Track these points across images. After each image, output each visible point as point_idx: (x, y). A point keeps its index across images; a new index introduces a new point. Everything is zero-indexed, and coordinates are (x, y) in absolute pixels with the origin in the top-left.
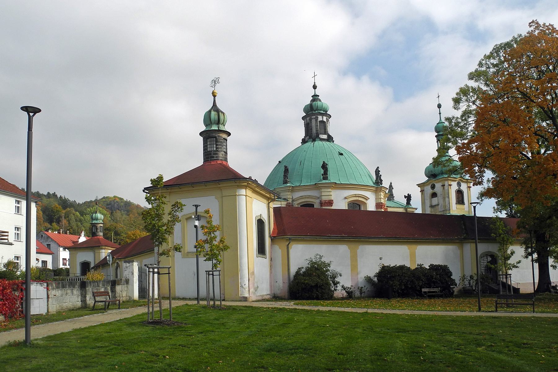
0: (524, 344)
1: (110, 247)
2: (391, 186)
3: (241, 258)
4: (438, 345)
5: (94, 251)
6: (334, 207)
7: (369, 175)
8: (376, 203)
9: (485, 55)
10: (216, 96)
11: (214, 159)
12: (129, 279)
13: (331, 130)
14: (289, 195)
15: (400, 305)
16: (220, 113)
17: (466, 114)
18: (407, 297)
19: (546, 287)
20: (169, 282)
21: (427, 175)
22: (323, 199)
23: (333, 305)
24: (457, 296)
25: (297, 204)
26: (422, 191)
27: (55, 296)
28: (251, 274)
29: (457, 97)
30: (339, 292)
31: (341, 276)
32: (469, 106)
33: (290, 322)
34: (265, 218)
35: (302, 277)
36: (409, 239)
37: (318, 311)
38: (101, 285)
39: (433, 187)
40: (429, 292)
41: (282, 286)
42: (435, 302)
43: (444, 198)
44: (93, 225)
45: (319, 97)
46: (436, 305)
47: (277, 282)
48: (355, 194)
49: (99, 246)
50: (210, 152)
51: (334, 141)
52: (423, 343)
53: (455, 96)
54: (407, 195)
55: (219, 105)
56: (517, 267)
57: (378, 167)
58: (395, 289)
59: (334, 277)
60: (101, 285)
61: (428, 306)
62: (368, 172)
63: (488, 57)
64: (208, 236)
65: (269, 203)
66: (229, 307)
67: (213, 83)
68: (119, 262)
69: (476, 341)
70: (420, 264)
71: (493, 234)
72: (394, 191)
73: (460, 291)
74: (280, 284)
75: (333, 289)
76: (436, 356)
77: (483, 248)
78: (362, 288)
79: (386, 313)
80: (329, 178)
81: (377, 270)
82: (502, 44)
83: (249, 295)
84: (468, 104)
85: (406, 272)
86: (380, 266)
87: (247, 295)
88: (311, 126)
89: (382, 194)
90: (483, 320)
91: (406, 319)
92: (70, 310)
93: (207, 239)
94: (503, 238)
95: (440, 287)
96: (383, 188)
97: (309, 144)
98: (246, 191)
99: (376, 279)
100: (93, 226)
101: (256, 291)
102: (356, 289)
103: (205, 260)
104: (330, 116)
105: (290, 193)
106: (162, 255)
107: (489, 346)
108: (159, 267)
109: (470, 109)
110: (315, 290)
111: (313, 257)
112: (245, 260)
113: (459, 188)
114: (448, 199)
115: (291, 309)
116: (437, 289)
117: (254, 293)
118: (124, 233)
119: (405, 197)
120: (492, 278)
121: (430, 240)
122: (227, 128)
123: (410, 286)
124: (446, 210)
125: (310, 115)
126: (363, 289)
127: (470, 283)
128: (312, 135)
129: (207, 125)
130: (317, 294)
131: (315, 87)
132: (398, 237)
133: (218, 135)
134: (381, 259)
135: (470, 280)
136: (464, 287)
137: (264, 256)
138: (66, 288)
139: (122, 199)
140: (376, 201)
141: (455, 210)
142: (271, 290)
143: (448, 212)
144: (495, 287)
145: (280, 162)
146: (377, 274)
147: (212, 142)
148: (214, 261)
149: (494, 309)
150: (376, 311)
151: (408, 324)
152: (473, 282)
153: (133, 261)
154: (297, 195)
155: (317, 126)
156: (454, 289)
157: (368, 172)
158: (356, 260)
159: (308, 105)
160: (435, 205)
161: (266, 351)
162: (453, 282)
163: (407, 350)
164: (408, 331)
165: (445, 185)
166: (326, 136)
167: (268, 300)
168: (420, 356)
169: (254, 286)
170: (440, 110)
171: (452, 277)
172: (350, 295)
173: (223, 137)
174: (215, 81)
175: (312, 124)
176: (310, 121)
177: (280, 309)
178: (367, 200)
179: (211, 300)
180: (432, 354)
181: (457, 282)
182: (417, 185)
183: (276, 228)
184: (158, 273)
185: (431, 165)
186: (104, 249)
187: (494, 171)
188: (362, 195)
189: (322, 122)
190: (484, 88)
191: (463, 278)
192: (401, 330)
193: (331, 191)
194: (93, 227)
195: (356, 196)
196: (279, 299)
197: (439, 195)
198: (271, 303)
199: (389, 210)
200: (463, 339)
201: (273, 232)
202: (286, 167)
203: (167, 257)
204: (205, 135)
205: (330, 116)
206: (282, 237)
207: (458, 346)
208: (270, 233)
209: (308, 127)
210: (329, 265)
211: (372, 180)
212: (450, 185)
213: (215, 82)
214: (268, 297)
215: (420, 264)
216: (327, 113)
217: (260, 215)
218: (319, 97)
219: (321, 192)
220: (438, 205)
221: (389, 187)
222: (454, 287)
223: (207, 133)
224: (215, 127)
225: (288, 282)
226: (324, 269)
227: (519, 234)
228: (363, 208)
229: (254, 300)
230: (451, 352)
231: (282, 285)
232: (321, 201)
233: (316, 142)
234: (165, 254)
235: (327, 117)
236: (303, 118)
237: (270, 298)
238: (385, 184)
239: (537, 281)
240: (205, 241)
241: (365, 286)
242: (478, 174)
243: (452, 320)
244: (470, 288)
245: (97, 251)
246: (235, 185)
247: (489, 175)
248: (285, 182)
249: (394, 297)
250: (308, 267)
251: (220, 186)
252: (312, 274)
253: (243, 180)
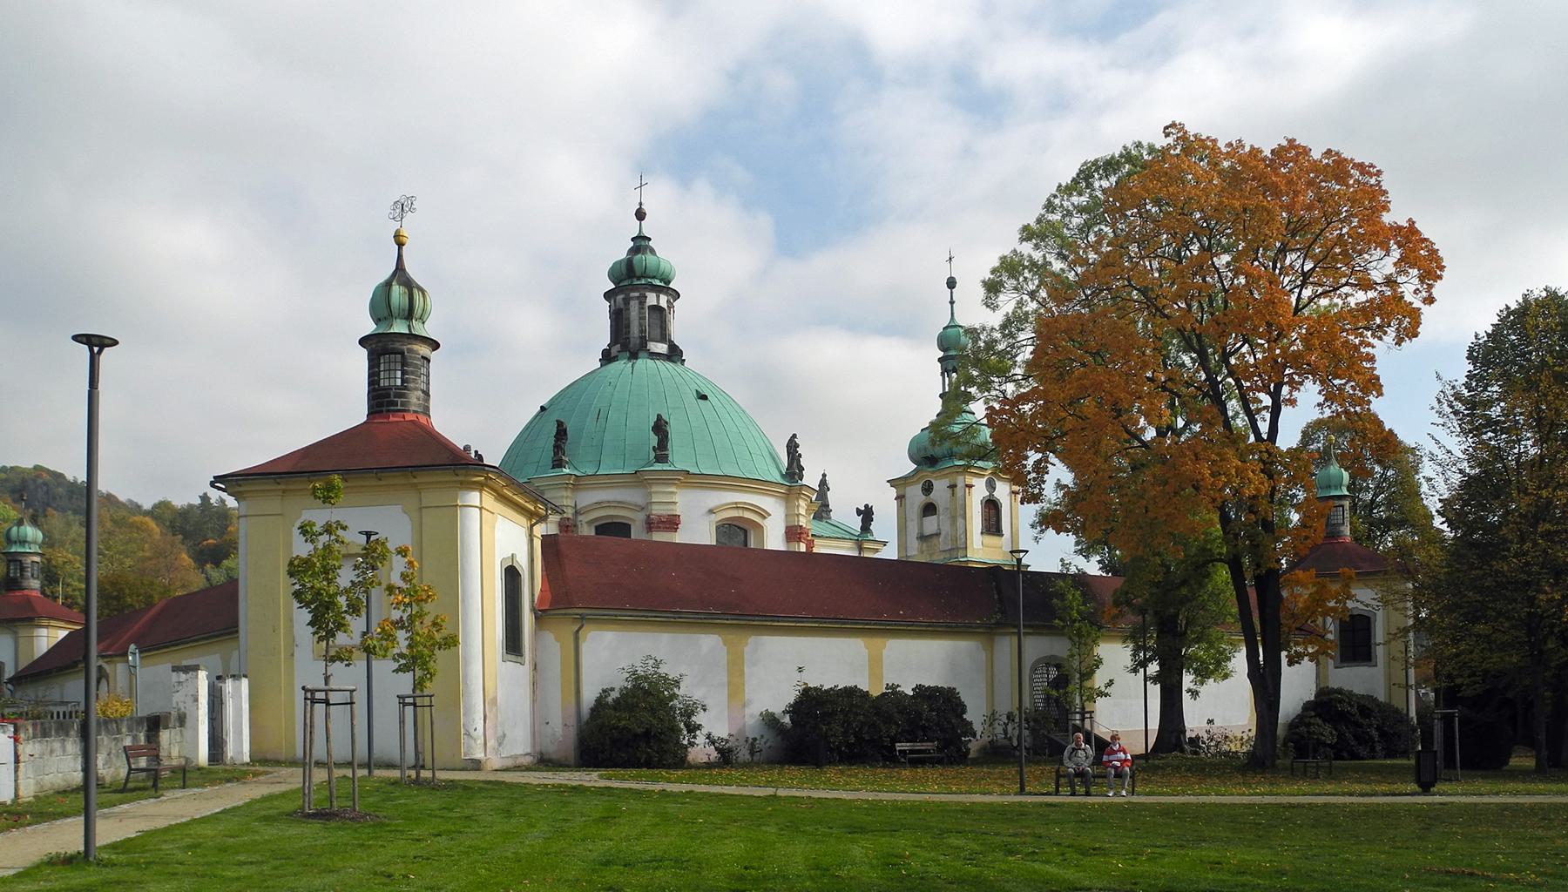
0: (1094, 849)
1: (62, 621)
2: (823, 483)
3: (466, 664)
4: (933, 854)
5: (16, 633)
6: (680, 537)
7: (770, 453)
8: (787, 528)
9: (1060, 186)
10: (403, 245)
11: (396, 408)
12: (185, 714)
13: (677, 333)
14: (567, 497)
15: (848, 779)
16: (415, 291)
17: (1010, 325)
18: (862, 763)
19: (1174, 741)
20: (352, 724)
21: (915, 457)
22: (654, 512)
23: (691, 780)
24: (976, 762)
25: (587, 523)
26: (900, 498)
27: (32, 758)
28: (490, 702)
29: (993, 279)
30: (701, 752)
31: (705, 710)
32: (1020, 304)
33: (616, 815)
34: (522, 563)
35: (612, 712)
36: (867, 624)
37: (663, 793)
38: (124, 730)
39: (928, 488)
40: (912, 752)
41: (560, 732)
42: (925, 774)
43: (954, 519)
44: (10, 558)
45: (651, 243)
46: (927, 781)
47: (547, 723)
48: (736, 503)
49: (32, 619)
50: (386, 389)
51: (684, 360)
52: (905, 850)
53: (988, 276)
54: (863, 509)
55: (411, 269)
56: (1106, 695)
57: (794, 436)
58: (834, 743)
59: (688, 713)
60: (124, 730)
61: (911, 782)
62: (768, 444)
63: (1067, 190)
64: (404, 611)
65: (532, 526)
66: (452, 785)
67: (397, 211)
68: (106, 666)
69: (1006, 846)
70: (893, 684)
71: (1057, 621)
72: (831, 497)
73: (983, 749)
74: (556, 730)
75: (685, 742)
76: (930, 869)
77: (1037, 647)
78: (755, 739)
79: (819, 798)
80: (670, 458)
81: (791, 696)
82: (1096, 161)
83: (486, 756)
84: (1018, 299)
85: (859, 704)
86: (799, 688)
87: (479, 755)
88: (628, 319)
89: (802, 503)
90: (1026, 809)
91: (865, 808)
92: (59, 793)
93: (401, 617)
94: (1079, 629)
95: (938, 739)
96: (804, 488)
97: (621, 366)
98: (481, 495)
99: (787, 720)
100: (10, 561)
101: (500, 744)
102: (742, 741)
103: (396, 671)
104: (677, 295)
105: (569, 493)
106: (334, 661)
107: (1028, 854)
108: (327, 688)
109: (1025, 309)
110: (643, 745)
111: (638, 664)
112: (476, 669)
113: (991, 495)
114: (963, 521)
115: (600, 788)
116: (931, 744)
117: (497, 751)
118: (75, 578)
119: (859, 512)
120: (1057, 720)
121: (917, 626)
122: (428, 329)
123: (1104, 760)
124: (958, 548)
125: (625, 288)
126: (758, 742)
127: (1005, 732)
128: (629, 342)
129: (379, 320)
130: (648, 753)
131: (640, 215)
132: (842, 617)
133: (409, 346)
134: (800, 670)
135: (1006, 725)
136: (992, 740)
137: (519, 659)
138: (50, 736)
139: (61, 476)
140: (787, 521)
141: (981, 550)
142: (534, 745)
143: (961, 553)
144: (1063, 740)
145: (543, 408)
146: (791, 706)
147: (392, 365)
148: (419, 673)
149: (1052, 788)
150: (794, 792)
151: (870, 818)
152: (1014, 728)
153: (196, 668)
154: (587, 498)
155: (642, 318)
156: (969, 746)
157: (768, 444)
158: (742, 674)
159: (621, 261)
160: (931, 536)
161: (602, 865)
162: (968, 729)
163: (874, 862)
164: (872, 831)
165: (956, 486)
166: (666, 346)
167: (528, 769)
168: (899, 869)
169: (496, 732)
170: (952, 293)
171: (965, 716)
172: (726, 757)
173: (421, 353)
174: (403, 205)
175: (629, 314)
176: (625, 304)
177: (574, 788)
178: (765, 518)
179: (361, 766)
180: (923, 866)
181: (978, 727)
182: (888, 481)
183: (548, 589)
184: (414, 705)
185: (927, 432)
186: (47, 627)
187: (1072, 467)
188: (752, 505)
189: (657, 309)
190: (1057, 266)
191: (992, 719)
192: (857, 829)
193: (675, 490)
194: (12, 564)
195: (737, 506)
196: (553, 767)
197: (940, 509)
198: (537, 774)
199: (821, 548)
200: (981, 844)
201: (541, 598)
202: (560, 424)
203: (346, 665)
204: (374, 346)
205: (677, 295)
206: (563, 612)
207: (970, 854)
208: (533, 601)
209: (618, 319)
210: (677, 683)
211: (778, 468)
212: (970, 486)
213: (403, 208)
214: (527, 760)
215: (893, 684)
216: (670, 286)
217: (510, 555)
218: (651, 243)
219: (650, 493)
220: (938, 535)
221: (819, 486)
222: (970, 740)
223: (380, 341)
224: (399, 327)
225: (575, 725)
226: (666, 693)
227: (1118, 618)
228: (754, 543)
229: (496, 767)
230: (959, 864)
231: (561, 730)
232: (648, 516)
233: (640, 361)
234: (342, 660)
235: (670, 297)
236: (608, 295)
237: (532, 762)
238: (811, 479)
239: (1154, 725)
240: (397, 623)
241: (762, 736)
242: (1034, 475)
243: (962, 811)
244: (1006, 742)
245: (23, 632)
246: (455, 482)
247: (1059, 474)
248: (558, 464)
249: (830, 763)
250: (626, 688)
251: (415, 481)
252: (638, 706)
253: (475, 469)
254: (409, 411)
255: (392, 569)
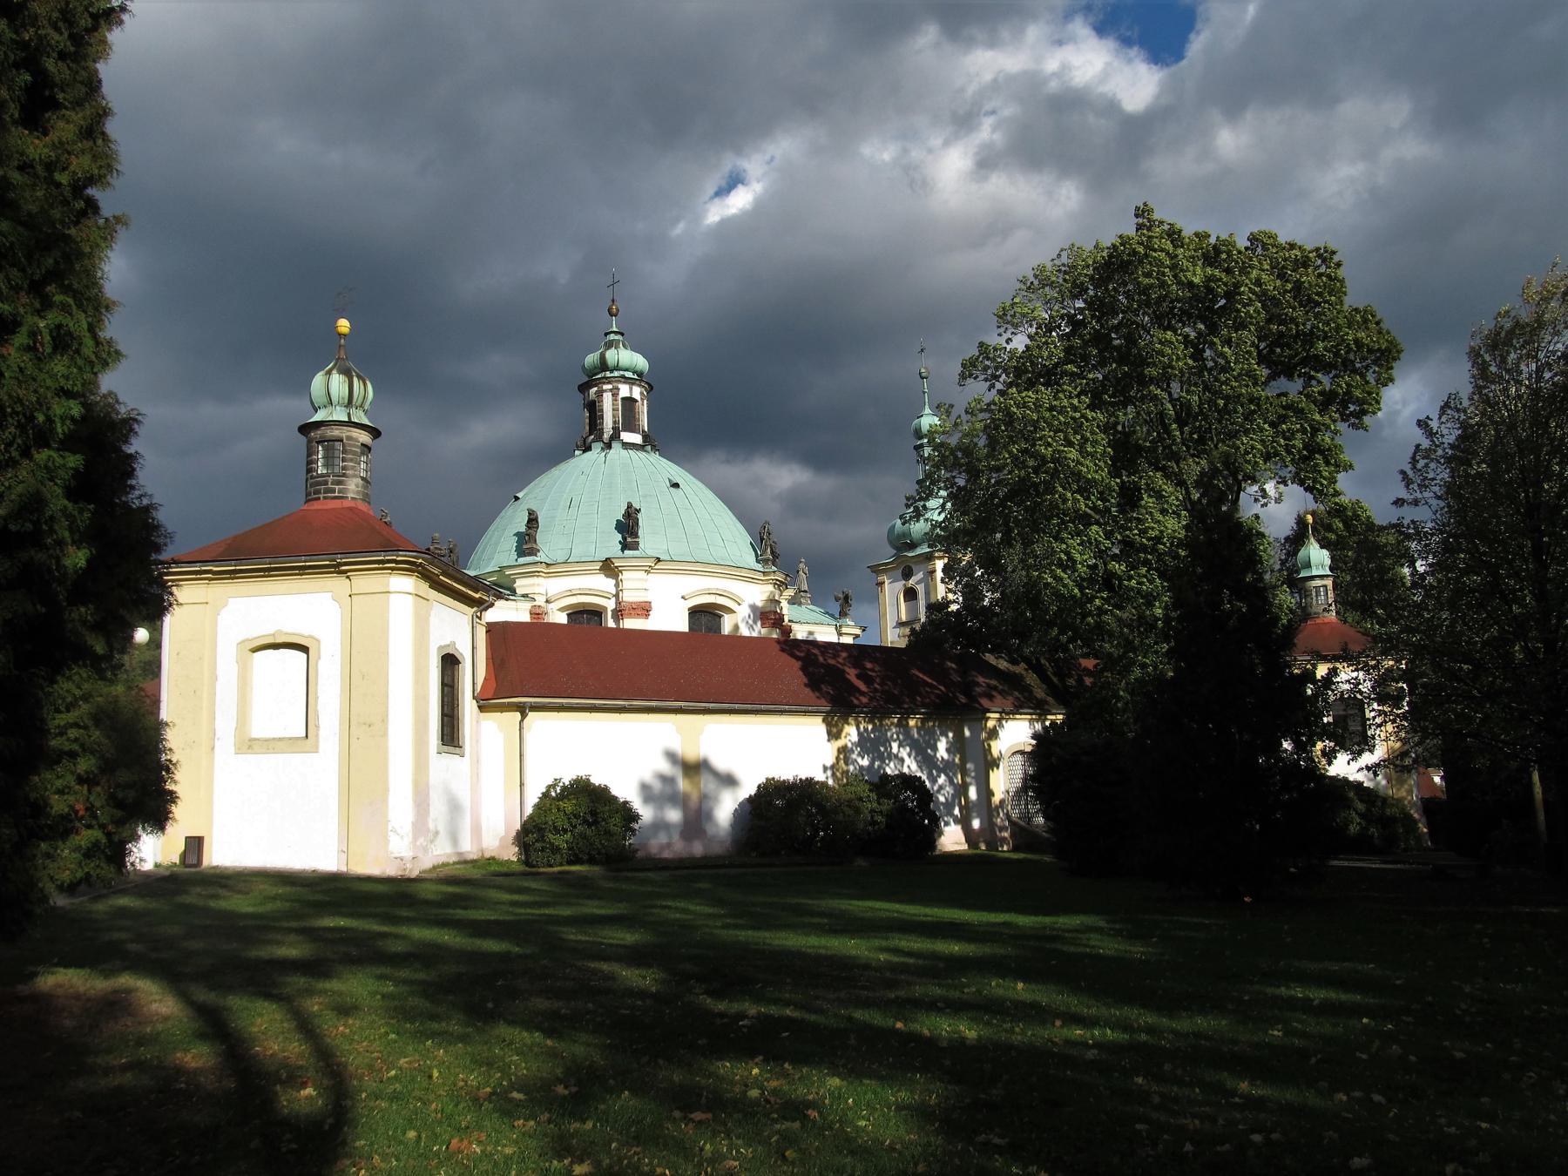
34: (464, 650)
48: (709, 589)
178: (739, 604)
254: (347, 497)
255: (320, 658)
